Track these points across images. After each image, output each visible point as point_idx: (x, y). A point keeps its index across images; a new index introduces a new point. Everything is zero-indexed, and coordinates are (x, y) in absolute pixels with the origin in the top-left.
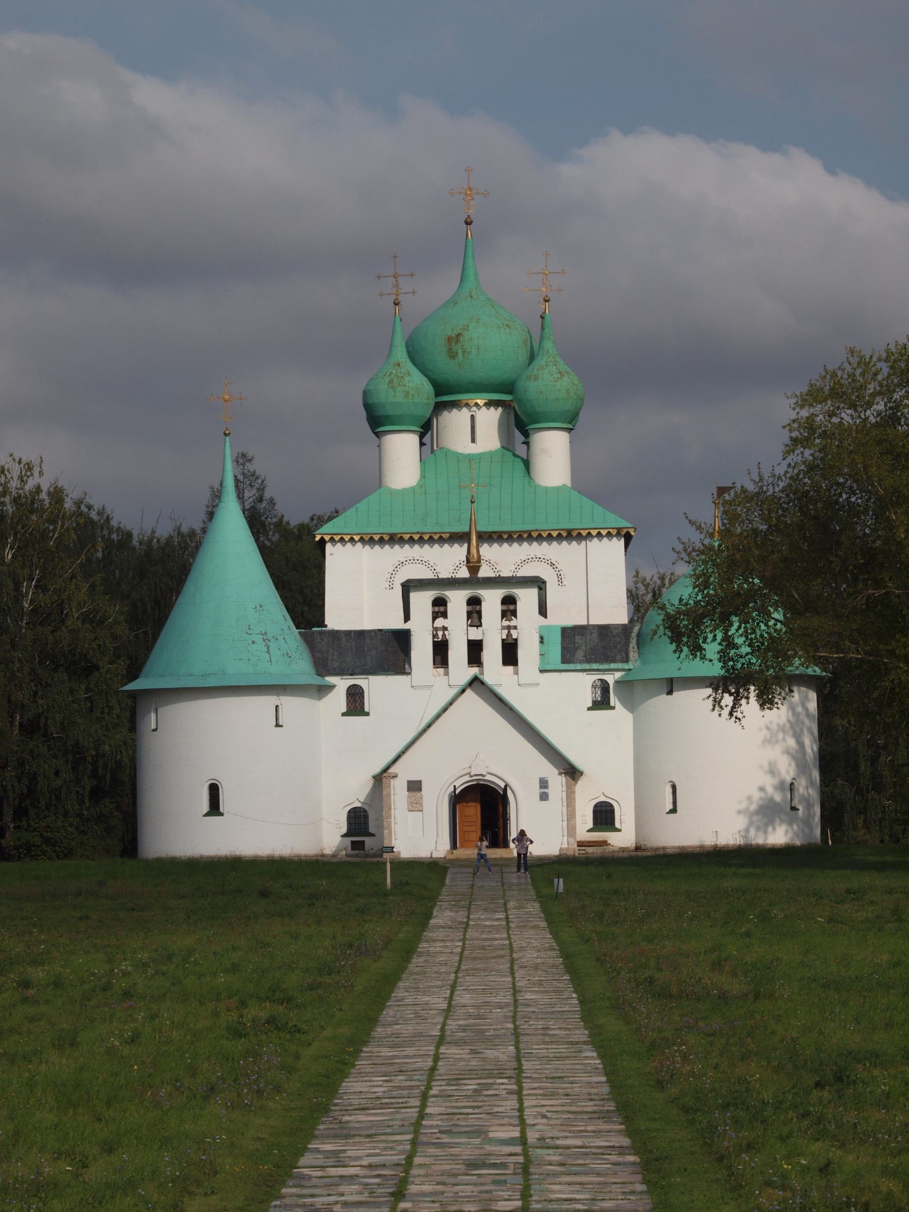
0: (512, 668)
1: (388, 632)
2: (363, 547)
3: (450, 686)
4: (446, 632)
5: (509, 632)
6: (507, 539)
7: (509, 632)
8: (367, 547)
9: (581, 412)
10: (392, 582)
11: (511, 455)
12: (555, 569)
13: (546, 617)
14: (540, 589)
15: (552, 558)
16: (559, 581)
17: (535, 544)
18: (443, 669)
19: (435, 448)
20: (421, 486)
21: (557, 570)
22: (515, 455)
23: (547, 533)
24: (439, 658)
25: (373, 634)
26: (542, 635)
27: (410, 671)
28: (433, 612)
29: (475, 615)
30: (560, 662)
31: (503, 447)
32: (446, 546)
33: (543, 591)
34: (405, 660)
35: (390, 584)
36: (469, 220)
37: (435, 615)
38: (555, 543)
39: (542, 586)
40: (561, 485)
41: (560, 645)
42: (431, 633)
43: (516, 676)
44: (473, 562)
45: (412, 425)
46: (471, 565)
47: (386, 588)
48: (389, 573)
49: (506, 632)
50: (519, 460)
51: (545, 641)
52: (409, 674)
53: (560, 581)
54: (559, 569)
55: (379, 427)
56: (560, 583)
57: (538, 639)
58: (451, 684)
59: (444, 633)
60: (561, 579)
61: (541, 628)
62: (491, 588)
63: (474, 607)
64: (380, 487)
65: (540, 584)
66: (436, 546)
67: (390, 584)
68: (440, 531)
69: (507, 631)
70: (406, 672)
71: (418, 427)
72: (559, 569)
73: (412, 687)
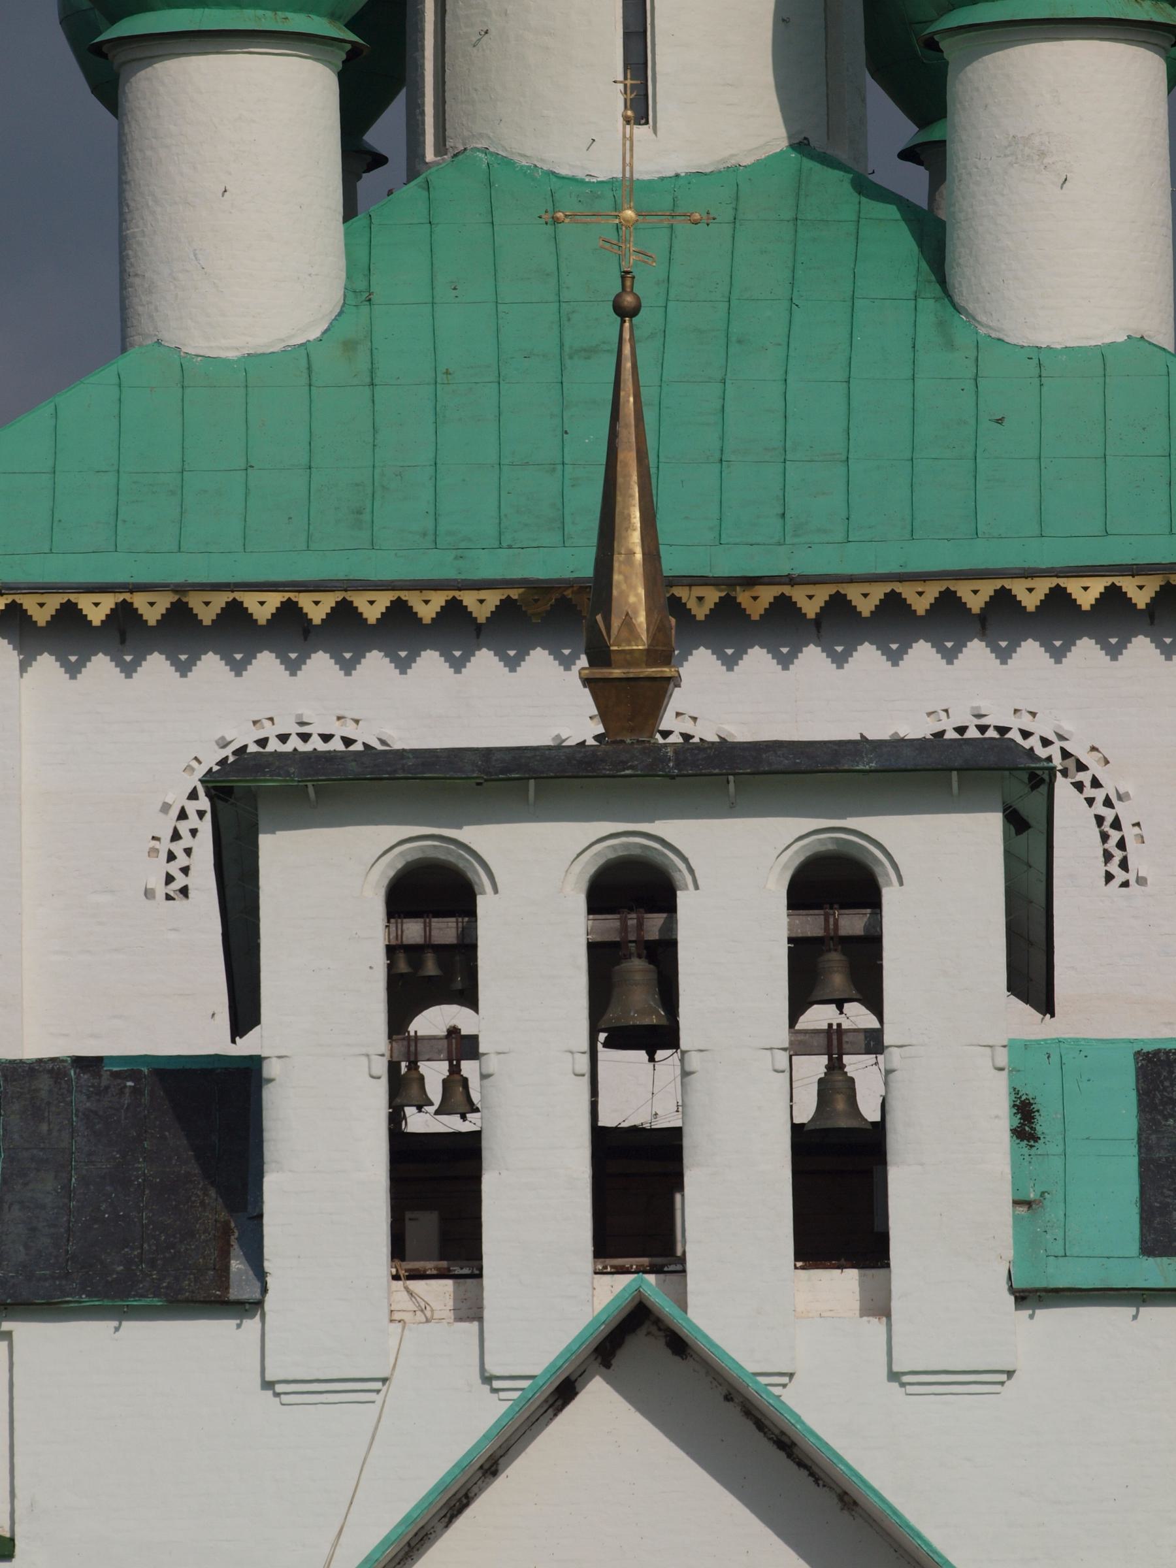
0: (851, 1276)
1: (134, 1075)
2: (24, 667)
3: (487, 1379)
4: (469, 1068)
5: (836, 1066)
6: (818, 622)
7: (836, 1066)
8: (46, 663)
9: (762, 1434)
10: (182, 860)
11: (847, 187)
12: (1089, 792)
13: (1046, 1005)
14: (1016, 822)
15: (1067, 727)
16: (1108, 856)
17: (976, 651)
18: (448, 1284)
19: (430, 156)
20: (349, 346)
21: (1099, 795)
22: (865, 187)
23: (1043, 586)
24: (425, 1225)
25: (44, 1083)
26: (1028, 1091)
27: (253, 1294)
28: (391, 950)
29: (637, 968)
30: (1134, 1247)
31: (801, 145)
32: (485, 660)
33: (1035, 837)
34: (226, 1232)
35: (174, 868)
36: (629, 300)
37: (403, 967)
38: (1086, 649)
39: (1030, 806)
40: (1121, 338)
41: (1134, 1150)
42: (381, 1067)
43: (876, 1326)
44: (630, 659)
45: (300, 9)
46: (617, 673)
47: (149, 894)
48: (166, 808)
49: (814, 1067)
50: (891, 211)
51: (1044, 1124)
52: (252, 1307)
53: (1118, 855)
54: (1109, 789)
55: (114, 20)
56: (1114, 867)
57: (1003, 1120)
58: (493, 1368)
59: (455, 1070)
60: (1121, 845)
61: (1020, 1049)
62: (732, 810)
63: (632, 921)
64: (124, 350)
65: (1017, 788)
66: (430, 661)
67: (174, 868)
68: (449, 573)
69: (824, 1060)
70: (234, 1294)
71: (333, 16)
72: (1109, 789)
73: (268, 1385)
